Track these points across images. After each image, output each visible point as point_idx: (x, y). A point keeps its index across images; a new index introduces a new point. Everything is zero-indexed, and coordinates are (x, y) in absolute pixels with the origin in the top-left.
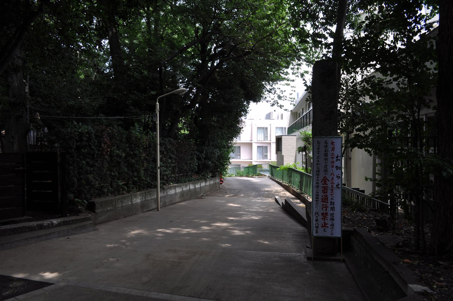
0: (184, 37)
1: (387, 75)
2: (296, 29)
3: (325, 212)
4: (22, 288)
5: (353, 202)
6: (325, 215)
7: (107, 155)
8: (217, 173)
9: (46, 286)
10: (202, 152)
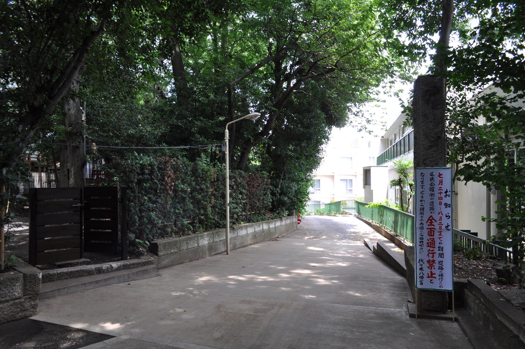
0: (255, 54)
1: (509, 91)
2: (389, 40)
3: (431, 259)
4: (81, 341)
5: (466, 247)
6: (431, 263)
7: (171, 189)
8: (294, 211)
9: (106, 339)
10: (276, 187)
